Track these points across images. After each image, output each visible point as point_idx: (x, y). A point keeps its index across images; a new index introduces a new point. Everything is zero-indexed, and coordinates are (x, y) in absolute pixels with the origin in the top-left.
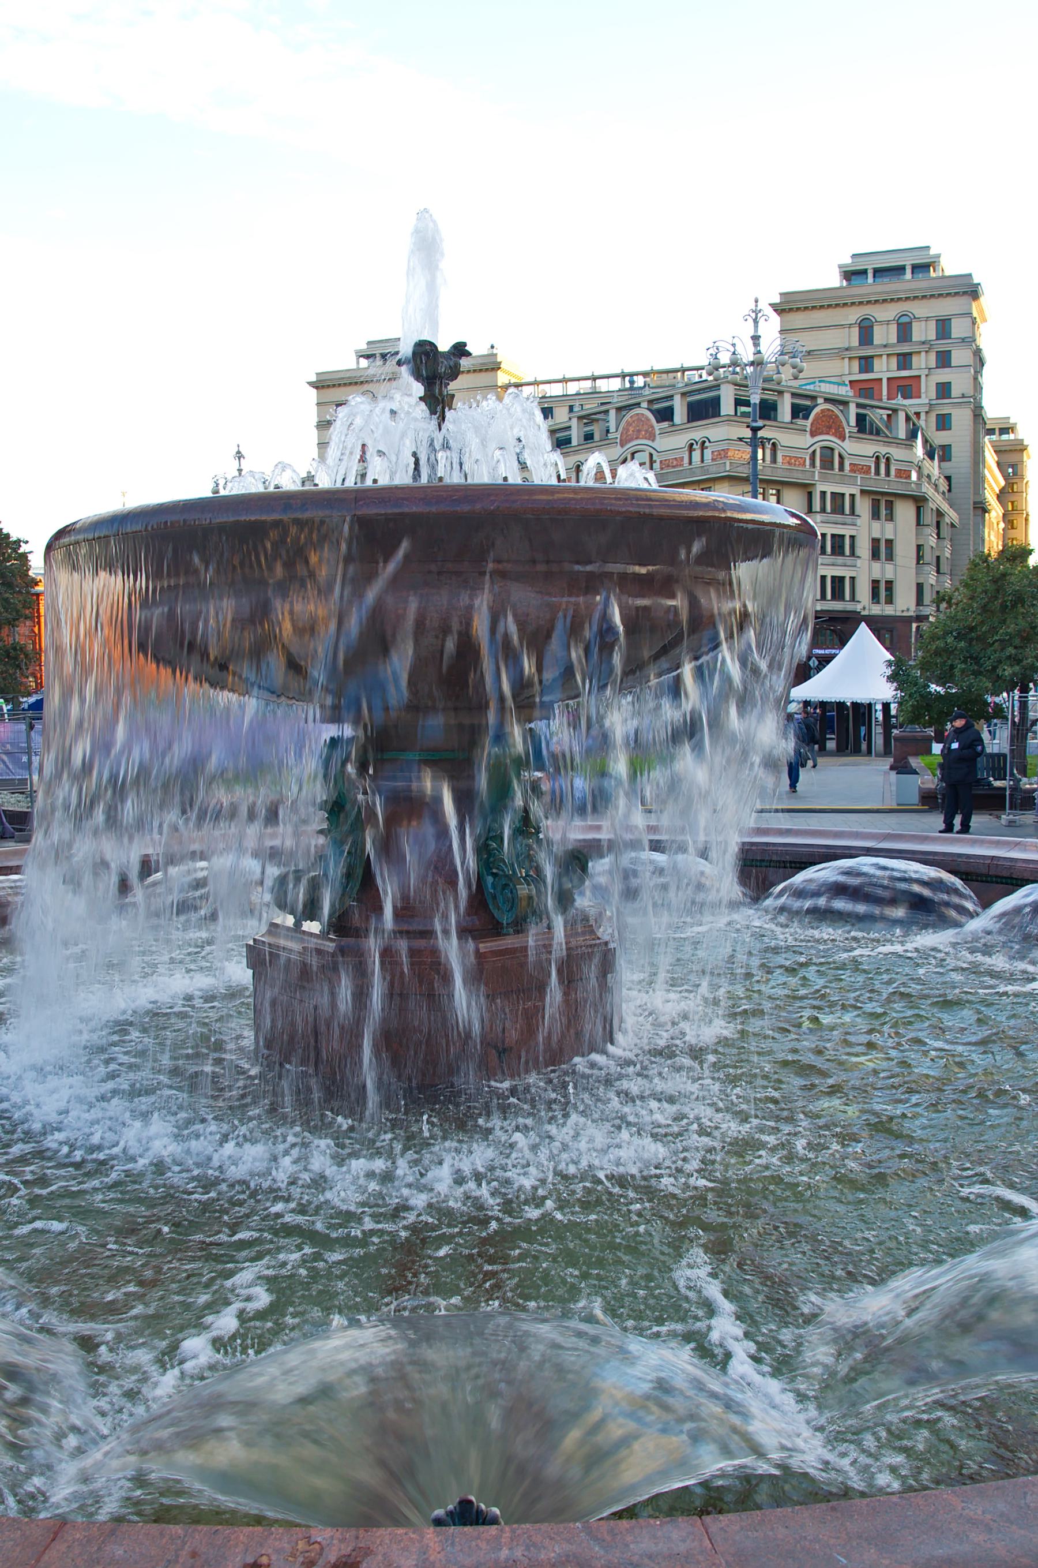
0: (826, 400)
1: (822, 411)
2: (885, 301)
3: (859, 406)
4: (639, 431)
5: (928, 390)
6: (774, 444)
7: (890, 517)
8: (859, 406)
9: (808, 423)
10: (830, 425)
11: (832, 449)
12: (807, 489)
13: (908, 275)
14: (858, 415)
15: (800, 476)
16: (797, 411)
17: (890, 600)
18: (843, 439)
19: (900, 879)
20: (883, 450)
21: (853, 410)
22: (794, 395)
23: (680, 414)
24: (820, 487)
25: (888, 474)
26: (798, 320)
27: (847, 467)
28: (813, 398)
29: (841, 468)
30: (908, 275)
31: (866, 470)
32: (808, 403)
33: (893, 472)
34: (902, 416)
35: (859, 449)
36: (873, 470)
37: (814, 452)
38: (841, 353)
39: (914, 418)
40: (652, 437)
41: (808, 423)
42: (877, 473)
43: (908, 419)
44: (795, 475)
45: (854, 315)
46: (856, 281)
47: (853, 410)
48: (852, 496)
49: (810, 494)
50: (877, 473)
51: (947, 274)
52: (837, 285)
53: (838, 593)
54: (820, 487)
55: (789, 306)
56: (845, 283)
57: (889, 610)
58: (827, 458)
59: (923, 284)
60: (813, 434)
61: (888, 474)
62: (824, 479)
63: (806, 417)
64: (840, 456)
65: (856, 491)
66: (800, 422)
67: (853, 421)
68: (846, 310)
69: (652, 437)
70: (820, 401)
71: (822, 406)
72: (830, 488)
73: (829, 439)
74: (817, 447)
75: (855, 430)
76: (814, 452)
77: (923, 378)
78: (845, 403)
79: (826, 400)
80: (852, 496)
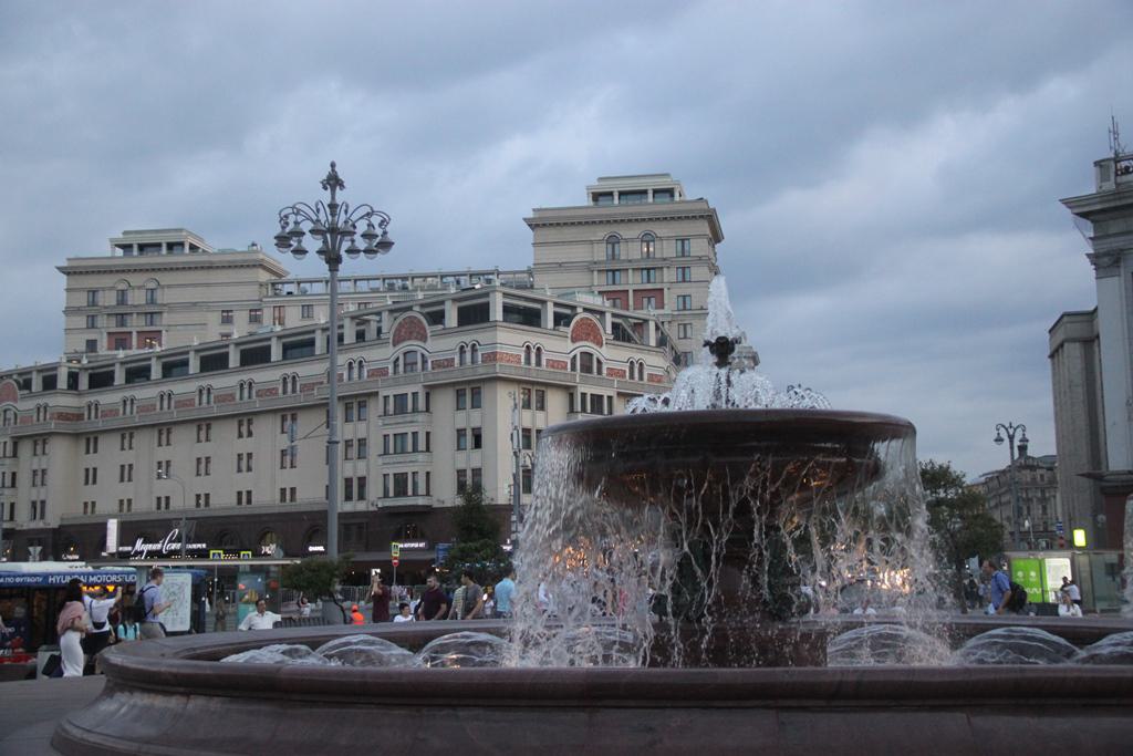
0: (585, 310)
1: (582, 319)
2: (630, 221)
3: (614, 315)
4: (411, 333)
5: (670, 298)
6: (641, 364)
7: (542, 407)
8: (614, 315)
9: (569, 330)
10: (588, 332)
11: (591, 355)
12: (569, 391)
13: (650, 198)
14: (613, 324)
15: (513, 371)
16: (560, 320)
17: (361, 497)
18: (600, 344)
19: (902, 706)
20: (637, 356)
21: (609, 319)
22: (556, 304)
23: (452, 319)
24: (581, 389)
25: (641, 378)
26: (551, 235)
27: (605, 372)
28: (573, 308)
29: (599, 372)
30: (650, 198)
31: (621, 374)
32: (568, 311)
33: (645, 377)
34: (652, 326)
35: (613, 355)
36: (627, 374)
37: (575, 357)
38: (590, 267)
39: (660, 325)
40: (424, 338)
41: (569, 330)
42: (632, 377)
43: (657, 328)
44: (507, 371)
45: (602, 233)
46: (603, 202)
47: (609, 319)
48: (610, 398)
49: (571, 396)
50: (632, 377)
51: (688, 198)
52: (586, 204)
53: (401, 490)
54: (581, 389)
55: (541, 223)
56: (591, 203)
57: (361, 506)
58: (587, 363)
59: (664, 208)
60: (574, 340)
61: (641, 378)
62: (584, 381)
63: (567, 325)
64: (599, 362)
65: (613, 393)
66: (562, 328)
67: (609, 330)
68: (593, 228)
69: (424, 338)
70: (579, 310)
71: (581, 315)
72: (590, 390)
73: (588, 346)
74: (577, 352)
75: (612, 337)
76: (575, 357)
77: (666, 290)
78: (602, 313)
79: (585, 310)
80: (610, 398)
